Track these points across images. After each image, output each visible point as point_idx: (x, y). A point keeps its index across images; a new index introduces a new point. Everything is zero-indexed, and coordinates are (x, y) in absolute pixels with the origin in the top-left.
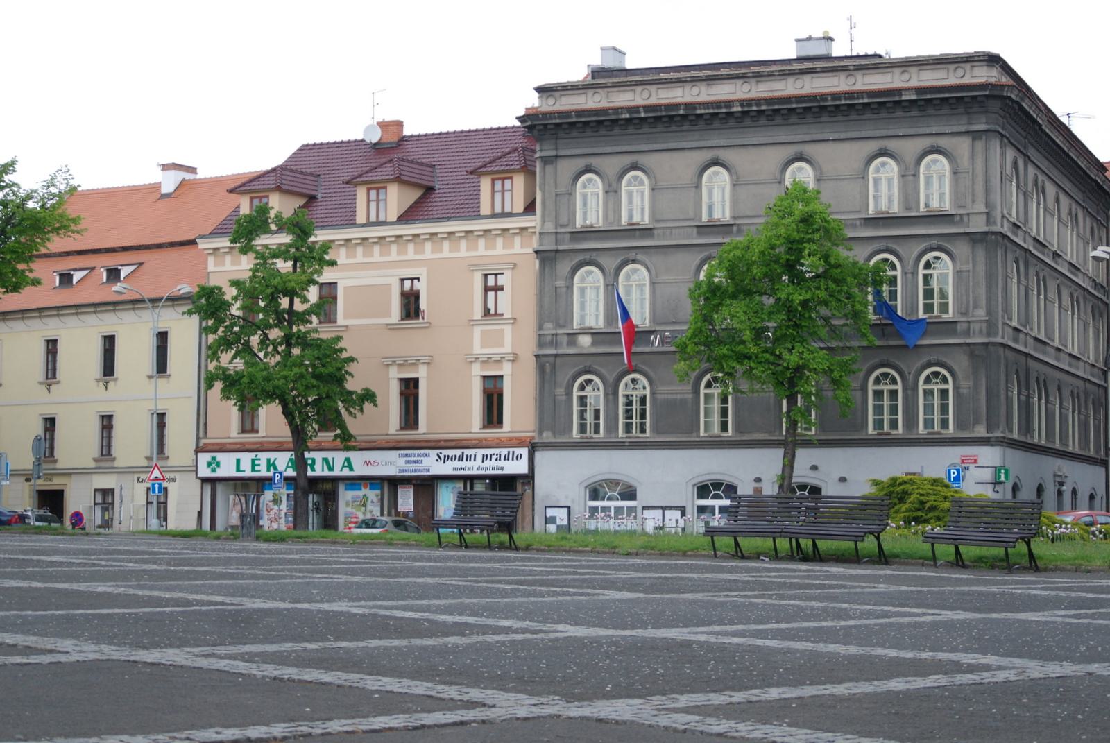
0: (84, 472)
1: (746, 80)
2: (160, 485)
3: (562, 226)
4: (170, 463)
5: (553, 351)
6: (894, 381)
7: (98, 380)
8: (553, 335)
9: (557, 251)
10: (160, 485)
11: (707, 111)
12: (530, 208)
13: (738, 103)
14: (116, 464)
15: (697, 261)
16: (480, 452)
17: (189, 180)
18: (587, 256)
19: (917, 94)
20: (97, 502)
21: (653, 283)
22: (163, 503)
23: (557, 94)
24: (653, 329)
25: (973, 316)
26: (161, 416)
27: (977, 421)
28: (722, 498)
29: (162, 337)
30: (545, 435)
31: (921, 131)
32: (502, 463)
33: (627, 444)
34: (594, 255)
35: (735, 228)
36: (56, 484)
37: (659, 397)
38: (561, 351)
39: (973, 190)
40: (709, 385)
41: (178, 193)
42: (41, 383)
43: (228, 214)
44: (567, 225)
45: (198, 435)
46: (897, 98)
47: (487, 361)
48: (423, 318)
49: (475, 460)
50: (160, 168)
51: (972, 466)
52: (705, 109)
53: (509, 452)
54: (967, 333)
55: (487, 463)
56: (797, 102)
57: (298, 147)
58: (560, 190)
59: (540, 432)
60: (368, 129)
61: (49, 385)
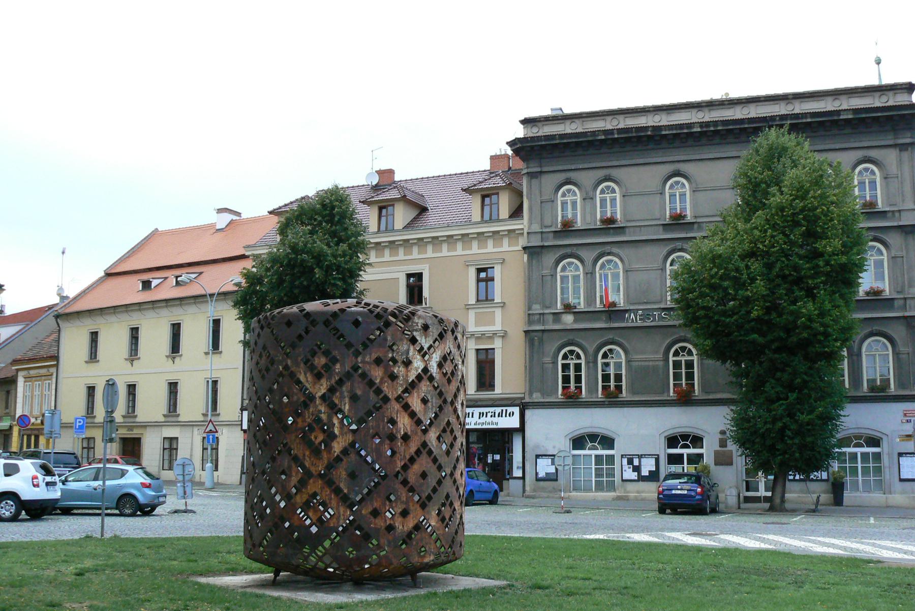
0: (157, 425)
1: (700, 109)
2: (213, 436)
3: (546, 227)
4: (221, 418)
5: (542, 328)
6: (578, 357)
7: (167, 357)
8: (540, 314)
9: (543, 247)
10: (213, 436)
11: (671, 132)
12: (516, 213)
13: (698, 125)
14: (180, 419)
15: (661, 257)
16: (477, 411)
17: (236, 220)
18: (569, 250)
20: (165, 447)
21: (626, 271)
22: (215, 449)
23: (540, 124)
24: (628, 308)
25: (909, 294)
26: (215, 383)
28: (690, 448)
29: (217, 323)
30: (534, 395)
32: (495, 419)
33: (606, 403)
34: (574, 250)
35: (696, 226)
36: (135, 433)
37: (634, 364)
38: (547, 327)
39: (903, 192)
40: (676, 354)
41: (228, 228)
42: (126, 359)
43: (263, 235)
44: (551, 226)
45: (242, 397)
46: (836, 118)
47: (481, 337)
48: (426, 304)
49: (472, 417)
50: (215, 212)
52: (669, 130)
53: (502, 410)
54: (904, 308)
55: (483, 419)
56: (749, 123)
58: (545, 198)
59: (531, 394)
60: (369, 175)
61: (132, 361)
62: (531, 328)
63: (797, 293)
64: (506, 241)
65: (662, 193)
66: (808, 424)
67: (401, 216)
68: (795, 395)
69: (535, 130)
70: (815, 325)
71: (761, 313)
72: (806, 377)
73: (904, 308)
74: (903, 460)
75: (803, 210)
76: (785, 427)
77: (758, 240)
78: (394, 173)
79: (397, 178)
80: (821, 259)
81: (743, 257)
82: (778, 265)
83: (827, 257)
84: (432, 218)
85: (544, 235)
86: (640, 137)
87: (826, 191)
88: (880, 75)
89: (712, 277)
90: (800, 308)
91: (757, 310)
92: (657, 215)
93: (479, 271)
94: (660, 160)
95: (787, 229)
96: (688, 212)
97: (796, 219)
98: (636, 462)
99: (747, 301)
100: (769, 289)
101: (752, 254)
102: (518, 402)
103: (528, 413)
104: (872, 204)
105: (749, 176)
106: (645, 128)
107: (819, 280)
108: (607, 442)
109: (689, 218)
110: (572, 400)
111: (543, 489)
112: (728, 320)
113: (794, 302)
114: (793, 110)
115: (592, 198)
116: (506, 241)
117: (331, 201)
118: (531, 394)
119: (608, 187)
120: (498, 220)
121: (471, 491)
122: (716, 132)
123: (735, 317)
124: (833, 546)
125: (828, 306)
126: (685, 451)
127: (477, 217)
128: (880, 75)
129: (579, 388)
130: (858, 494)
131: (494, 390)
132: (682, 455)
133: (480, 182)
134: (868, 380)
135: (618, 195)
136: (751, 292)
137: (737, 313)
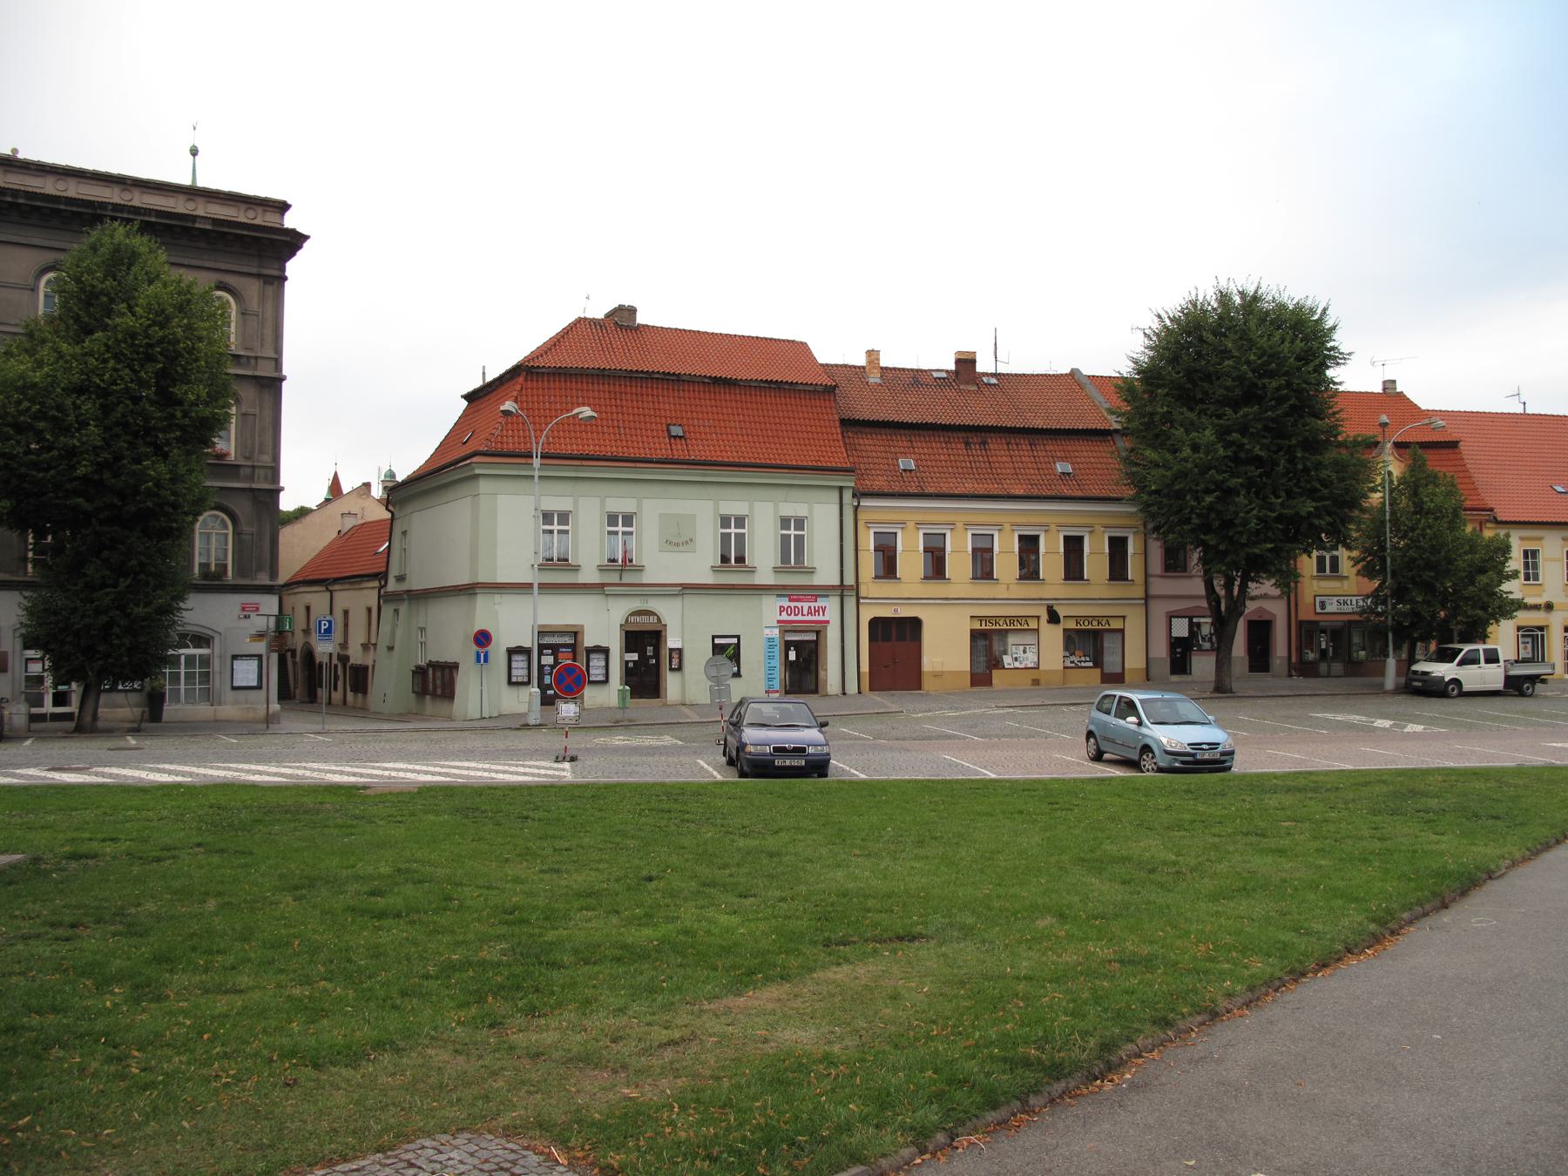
19: (213, 225)
27: (260, 569)
31: (207, 264)
39: (262, 334)
46: (190, 224)
51: (253, 615)
56: (66, 204)
57: (571, 319)
63: (143, 449)
65: (34, 289)
66: (143, 619)
68: (129, 581)
70: (163, 493)
71: (90, 469)
72: (143, 558)
73: (251, 478)
74: (237, 664)
75: (161, 341)
77: (92, 371)
78: (1078, 370)
79: (641, 319)
80: (177, 408)
81: (69, 391)
82: (120, 409)
87: (194, 320)
89: (21, 413)
90: (147, 468)
91: (85, 466)
95: (136, 363)
97: (150, 351)
99: (71, 454)
100: (104, 439)
101: (80, 390)
105: (82, 282)
107: (172, 435)
112: (41, 475)
113: (138, 461)
114: (130, 200)
123: (52, 472)
124: (177, 773)
125: (182, 470)
130: (178, 707)
134: (200, 564)
136: (79, 441)
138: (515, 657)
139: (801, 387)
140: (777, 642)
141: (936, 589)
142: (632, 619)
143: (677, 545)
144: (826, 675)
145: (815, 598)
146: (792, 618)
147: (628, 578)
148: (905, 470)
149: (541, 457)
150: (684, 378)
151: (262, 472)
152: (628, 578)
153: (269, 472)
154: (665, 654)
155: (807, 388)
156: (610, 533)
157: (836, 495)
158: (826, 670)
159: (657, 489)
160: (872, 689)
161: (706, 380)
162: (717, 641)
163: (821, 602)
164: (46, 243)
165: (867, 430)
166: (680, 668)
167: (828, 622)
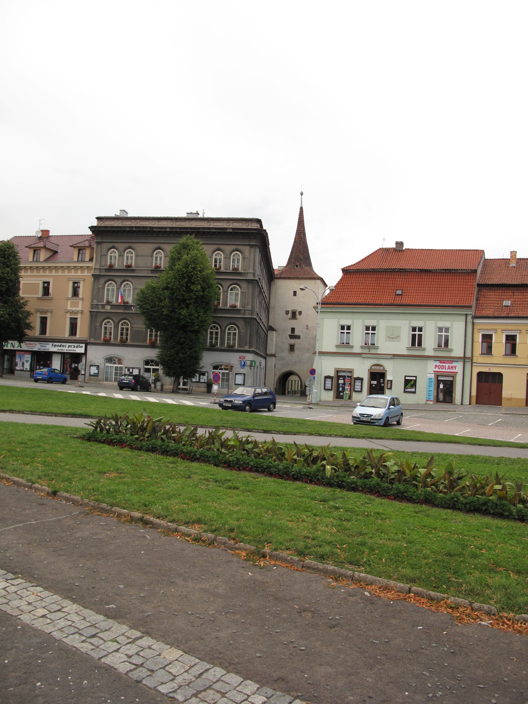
3: (102, 266)
5: (96, 310)
8: (96, 304)
9: (100, 275)
12: (91, 260)
16: (68, 344)
18: (111, 278)
19: (232, 230)
21: (134, 289)
27: (246, 344)
31: (232, 243)
32: (74, 349)
38: (99, 310)
46: (225, 231)
47: (72, 312)
54: (244, 314)
55: (70, 348)
58: (103, 253)
59: (90, 339)
62: (92, 310)
64: (86, 271)
65: (152, 256)
67: (43, 255)
69: (101, 223)
76: (175, 359)
81: (163, 289)
83: (194, 292)
84: (59, 256)
85: (101, 270)
86: (145, 231)
88: (302, 201)
92: (149, 265)
93: (74, 283)
94: (152, 241)
96: (162, 265)
98: (131, 370)
99: (163, 307)
101: (167, 288)
102: (85, 342)
103: (89, 347)
104: (237, 269)
106: (146, 227)
108: (120, 361)
109: (162, 268)
110: (107, 343)
111: (92, 380)
115: (122, 256)
116: (86, 271)
117: (4, 248)
118: (90, 339)
119: (130, 251)
120: (84, 261)
121: (51, 377)
122: (176, 232)
126: (152, 367)
127: (75, 259)
128: (302, 201)
129: (127, 339)
131: (76, 336)
132: (150, 369)
133: (79, 243)
135: (134, 255)
137: (159, 312)
138: (327, 380)
139: (460, 271)
140: (433, 380)
141: (511, 360)
142: (373, 367)
143: (393, 338)
144: (455, 395)
145: (452, 362)
146: (441, 370)
147: (372, 351)
148: (505, 306)
149: (321, 304)
150: (408, 270)
151: (248, 312)
152: (372, 351)
153: (250, 312)
154: (386, 381)
155: (463, 271)
156: (341, 333)
157: (464, 318)
158: (455, 393)
159: (402, 316)
160: (477, 403)
161: (417, 271)
162: (407, 378)
163: (454, 364)
164: (210, 243)
165: (494, 288)
166: (391, 388)
167: (457, 373)
